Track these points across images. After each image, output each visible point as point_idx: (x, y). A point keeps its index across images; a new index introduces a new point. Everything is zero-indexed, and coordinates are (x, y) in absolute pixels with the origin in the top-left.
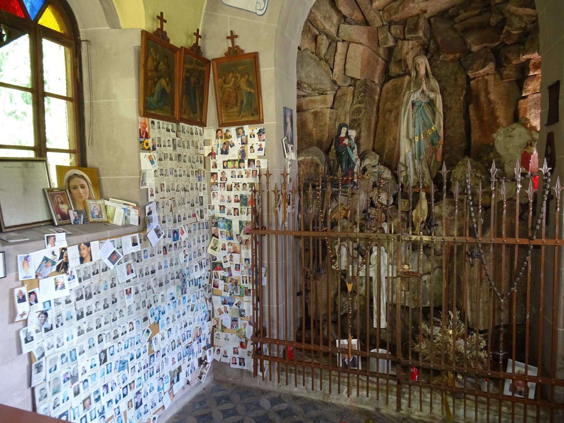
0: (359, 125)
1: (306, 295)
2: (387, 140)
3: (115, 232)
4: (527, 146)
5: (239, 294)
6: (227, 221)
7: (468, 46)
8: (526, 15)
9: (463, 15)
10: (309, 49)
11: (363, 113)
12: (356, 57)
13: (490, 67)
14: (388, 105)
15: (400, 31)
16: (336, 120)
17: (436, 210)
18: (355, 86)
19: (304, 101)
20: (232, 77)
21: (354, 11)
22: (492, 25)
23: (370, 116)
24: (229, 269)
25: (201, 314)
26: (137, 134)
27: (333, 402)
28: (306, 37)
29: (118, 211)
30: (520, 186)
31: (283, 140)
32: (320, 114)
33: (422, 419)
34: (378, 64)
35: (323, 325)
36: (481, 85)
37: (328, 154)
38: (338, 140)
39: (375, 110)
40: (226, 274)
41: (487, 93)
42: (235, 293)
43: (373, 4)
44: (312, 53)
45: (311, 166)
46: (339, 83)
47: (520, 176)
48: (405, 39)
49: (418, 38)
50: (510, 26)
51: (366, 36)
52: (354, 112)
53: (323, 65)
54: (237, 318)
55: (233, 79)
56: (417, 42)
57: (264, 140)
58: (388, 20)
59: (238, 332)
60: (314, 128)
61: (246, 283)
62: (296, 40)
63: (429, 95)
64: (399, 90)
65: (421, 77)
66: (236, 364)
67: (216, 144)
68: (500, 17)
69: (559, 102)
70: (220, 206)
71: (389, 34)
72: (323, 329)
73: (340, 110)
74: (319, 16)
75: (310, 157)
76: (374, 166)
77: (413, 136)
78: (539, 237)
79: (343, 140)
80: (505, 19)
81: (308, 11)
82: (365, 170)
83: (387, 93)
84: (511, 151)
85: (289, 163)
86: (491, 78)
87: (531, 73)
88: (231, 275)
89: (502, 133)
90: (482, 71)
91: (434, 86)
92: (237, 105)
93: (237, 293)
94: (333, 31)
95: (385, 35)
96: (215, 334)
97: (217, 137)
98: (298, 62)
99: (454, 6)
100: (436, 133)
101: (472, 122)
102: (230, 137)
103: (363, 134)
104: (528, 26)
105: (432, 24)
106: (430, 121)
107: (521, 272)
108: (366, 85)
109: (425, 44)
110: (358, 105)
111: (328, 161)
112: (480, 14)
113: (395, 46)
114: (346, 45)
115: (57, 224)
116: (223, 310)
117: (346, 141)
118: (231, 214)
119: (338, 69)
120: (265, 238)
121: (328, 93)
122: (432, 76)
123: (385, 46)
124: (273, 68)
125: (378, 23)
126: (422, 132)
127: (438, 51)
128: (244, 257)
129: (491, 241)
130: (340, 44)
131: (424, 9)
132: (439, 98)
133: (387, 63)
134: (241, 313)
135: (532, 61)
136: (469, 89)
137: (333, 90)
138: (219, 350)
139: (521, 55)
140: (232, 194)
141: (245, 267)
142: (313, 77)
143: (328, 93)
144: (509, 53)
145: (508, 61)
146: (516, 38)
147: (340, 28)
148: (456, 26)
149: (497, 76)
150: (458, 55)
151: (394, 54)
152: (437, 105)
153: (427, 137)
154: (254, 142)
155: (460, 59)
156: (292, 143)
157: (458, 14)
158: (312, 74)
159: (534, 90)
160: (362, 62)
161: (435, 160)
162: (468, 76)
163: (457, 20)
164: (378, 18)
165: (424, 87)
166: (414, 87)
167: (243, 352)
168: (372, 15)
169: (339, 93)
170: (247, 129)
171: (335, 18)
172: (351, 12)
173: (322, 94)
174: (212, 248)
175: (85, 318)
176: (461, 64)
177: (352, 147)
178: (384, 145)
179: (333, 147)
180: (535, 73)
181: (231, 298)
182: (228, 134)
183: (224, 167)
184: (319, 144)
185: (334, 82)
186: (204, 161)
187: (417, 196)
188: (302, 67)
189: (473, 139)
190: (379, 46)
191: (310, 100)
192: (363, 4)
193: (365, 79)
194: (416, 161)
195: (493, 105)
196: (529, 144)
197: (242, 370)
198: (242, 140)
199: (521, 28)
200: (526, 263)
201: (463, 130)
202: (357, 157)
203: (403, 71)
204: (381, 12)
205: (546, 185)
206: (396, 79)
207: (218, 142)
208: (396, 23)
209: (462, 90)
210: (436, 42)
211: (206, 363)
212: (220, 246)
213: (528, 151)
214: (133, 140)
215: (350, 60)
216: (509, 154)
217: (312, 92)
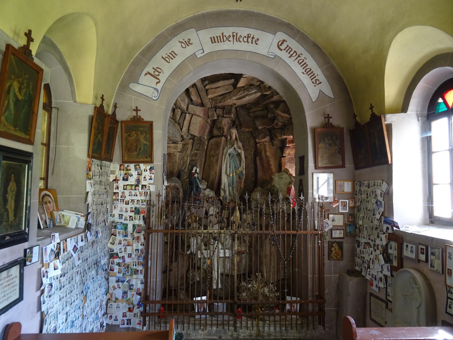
2: (211, 173)
3: (72, 233)
5: (130, 274)
6: (124, 224)
13: (267, 139)
14: (212, 153)
17: (244, 216)
20: (135, 134)
24: (123, 257)
25: (103, 290)
26: (86, 169)
27: (193, 338)
29: (73, 219)
30: (292, 205)
32: (172, 155)
33: (245, 337)
36: (262, 147)
39: (204, 155)
40: (121, 261)
41: (266, 152)
42: (127, 274)
45: (173, 189)
46: (185, 137)
48: (223, 117)
49: (231, 117)
50: (278, 120)
51: (203, 112)
52: (193, 155)
54: (127, 291)
55: (135, 135)
59: (127, 301)
61: (136, 266)
66: (124, 324)
67: (120, 174)
70: (119, 215)
73: (184, 153)
76: (205, 189)
78: (301, 230)
83: (212, 145)
84: (282, 186)
86: (267, 144)
87: (287, 145)
88: (124, 261)
92: (136, 151)
93: (128, 273)
94: (185, 107)
96: (109, 305)
97: (120, 169)
100: (242, 172)
101: (258, 166)
102: (130, 170)
108: (201, 140)
110: (195, 152)
112: (262, 110)
113: (217, 119)
114: (190, 115)
115: (42, 228)
116: (116, 287)
117: (196, 175)
118: (127, 220)
119: (185, 129)
120: (151, 235)
128: (135, 248)
130: (187, 115)
132: (243, 152)
134: (131, 287)
136: (256, 148)
138: (111, 316)
140: (129, 207)
141: (135, 255)
145: (277, 137)
148: (250, 114)
150: (251, 129)
154: (147, 174)
155: (252, 131)
161: (240, 187)
163: (251, 111)
164: (209, 103)
165: (236, 146)
167: (130, 315)
170: (142, 166)
171: (187, 100)
173: (175, 143)
174: (111, 243)
175: (62, 289)
176: (252, 134)
178: (209, 176)
181: (123, 277)
182: (129, 168)
183: (124, 189)
185: (182, 136)
186: (110, 185)
189: (259, 176)
190: (208, 118)
194: (230, 188)
196: (290, 183)
197: (128, 328)
198: (138, 173)
201: (253, 171)
207: (121, 172)
211: (104, 326)
212: (117, 242)
214: (81, 173)
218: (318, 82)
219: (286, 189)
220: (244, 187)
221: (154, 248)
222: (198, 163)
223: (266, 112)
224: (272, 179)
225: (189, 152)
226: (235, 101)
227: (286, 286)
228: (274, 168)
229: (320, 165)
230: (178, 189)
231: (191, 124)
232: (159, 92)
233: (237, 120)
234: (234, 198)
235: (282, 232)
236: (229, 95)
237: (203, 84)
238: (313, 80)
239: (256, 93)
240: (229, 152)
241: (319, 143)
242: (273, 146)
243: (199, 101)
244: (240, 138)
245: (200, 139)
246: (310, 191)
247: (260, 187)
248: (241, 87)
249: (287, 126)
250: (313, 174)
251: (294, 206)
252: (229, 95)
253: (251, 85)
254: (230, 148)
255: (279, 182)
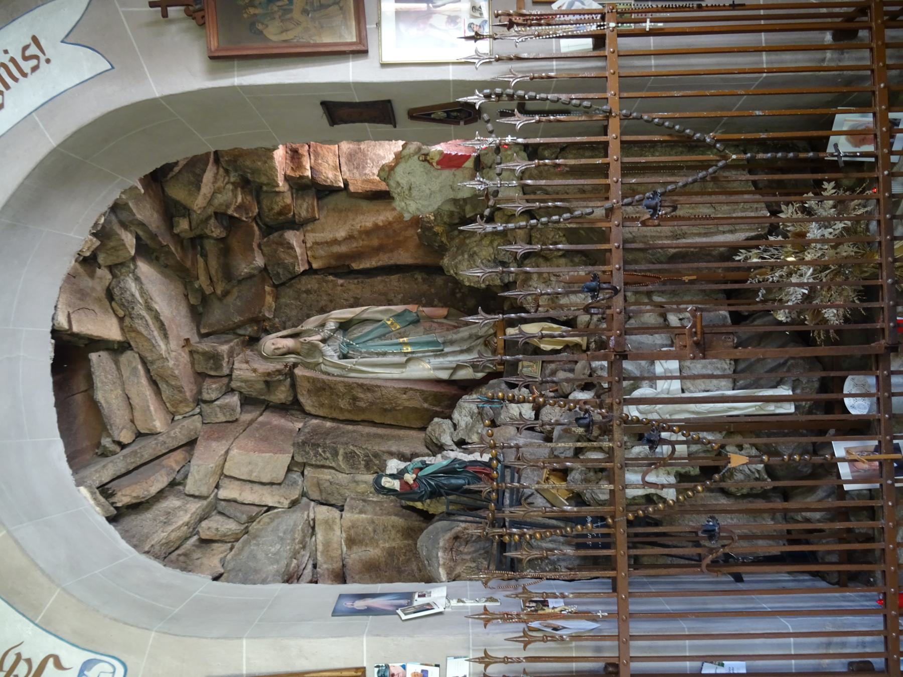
0: (376, 455)
1: (737, 564)
2: (407, 404)
4: (428, 161)
7: (256, 272)
8: (214, 182)
9: (203, 281)
10: (222, 555)
11: (355, 449)
12: (250, 461)
14: (343, 404)
15: (215, 383)
16: (364, 501)
18: (304, 465)
19: (324, 566)
21: (163, 467)
22: (224, 235)
23: (362, 435)
28: (199, 562)
31: (404, 617)
32: (352, 532)
34: (269, 423)
35: (798, 522)
36: (321, 252)
37: (433, 516)
38: (407, 492)
39: (350, 427)
41: (335, 242)
43: (159, 430)
44: (231, 549)
46: (295, 495)
47: (491, 140)
48: (230, 376)
49: (231, 354)
50: (228, 207)
51: (214, 444)
52: (353, 466)
53: (259, 526)
56: (238, 354)
57: (404, 667)
58: (192, 405)
60: (377, 546)
62: (198, 584)
63: (331, 330)
64: (318, 386)
65: (299, 345)
68: (212, 221)
69: (357, 101)
71: (216, 403)
72: (808, 520)
73: (347, 493)
74: (160, 536)
75: (440, 554)
76: (455, 426)
77: (402, 357)
79: (407, 483)
80: (216, 214)
81: (143, 558)
82: (461, 444)
83: (322, 405)
84: (435, 186)
85: (454, 603)
86: (311, 238)
87: (308, 173)
89: (403, 204)
90: (298, 250)
91: (317, 324)
94: (195, 507)
95: (218, 409)
98: (244, 582)
99: (186, 296)
100: (398, 316)
101: (380, 263)
103: (394, 449)
104: (232, 180)
105: (210, 330)
106: (376, 328)
107: (674, 127)
109: (243, 342)
110: (340, 458)
111: (448, 515)
112: (205, 256)
113: (241, 393)
114: (225, 482)
117: (409, 478)
119: (269, 499)
121: (312, 516)
122: (299, 328)
123: (239, 409)
124: (244, 642)
125: (196, 422)
126: (395, 341)
127: (256, 320)
129: (617, 182)
130: (223, 494)
131: (182, 343)
133: (268, 406)
135: (289, 172)
137: (308, 506)
139: (277, 189)
142: (278, 546)
143: (312, 516)
144: (272, 209)
146: (249, 198)
147: (192, 493)
148: (219, 292)
149: (309, 228)
150: (267, 288)
151: (254, 394)
152: (350, 316)
153: (405, 332)
155: (275, 286)
156: (409, 596)
157: (201, 290)
158: (273, 550)
159: (336, 169)
160: (260, 451)
161: (445, 318)
162: (305, 273)
163: (208, 290)
164: (186, 423)
165: (315, 338)
166: (315, 358)
168: (179, 434)
169: (315, 495)
171: (172, 502)
172: (163, 472)
173: (313, 528)
176: (283, 284)
177: (420, 465)
179: (419, 505)
180: (308, 167)
184: (411, 534)
185: (294, 503)
187: (510, 346)
188: (256, 571)
190: (237, 420)
191: (322, 552)
192: (154, 449)
193: (294, 445)
194: (446, 350)
195: (356, 233)
196: (426, 158)
199: (234, 191)
200: (656, 120)
202: (439, 456)
203: (285, 380)
204: (176, 418)
205: (508, 95)
206: (299, 390)
208: (200, 392)
209: (327, 282)
210: (241, 325)
213: (437, 158)
215: (254, 474)
216: (440, 191)
217: (308, 549)
218: (33, 50)
219: (447, 173)
220: (445, 305)
221: (678, 648)
222: (376, 448)
223: (209, 245)
224: (417, 221)
225: (342, 478)
226: (173, 344)
227: (802, 155)
228: (373, 217)
229: (349, 36)
230: (456, 538)
231: (253, 478)
232: (92, 656)
233: (241, 332)
234: (479, 338)
235: (615, 176)
236: (152, 363)
237: (114, 453)
238: (27, 70)
239: (137, 279)
240: (335, 360)
241: (266, 39)
242: (314, 220)
243: (179, 455)
244: (288, 323)
245: (301, 446)
246: (451, 74)
247: (442, 259)
248: (122, 329)
249: (244, 169)
250: (384, 65)
251: (512, 130)
252: (152, 363)
253: (110, 295)
254: (322, 354)
255: (424, 196)
